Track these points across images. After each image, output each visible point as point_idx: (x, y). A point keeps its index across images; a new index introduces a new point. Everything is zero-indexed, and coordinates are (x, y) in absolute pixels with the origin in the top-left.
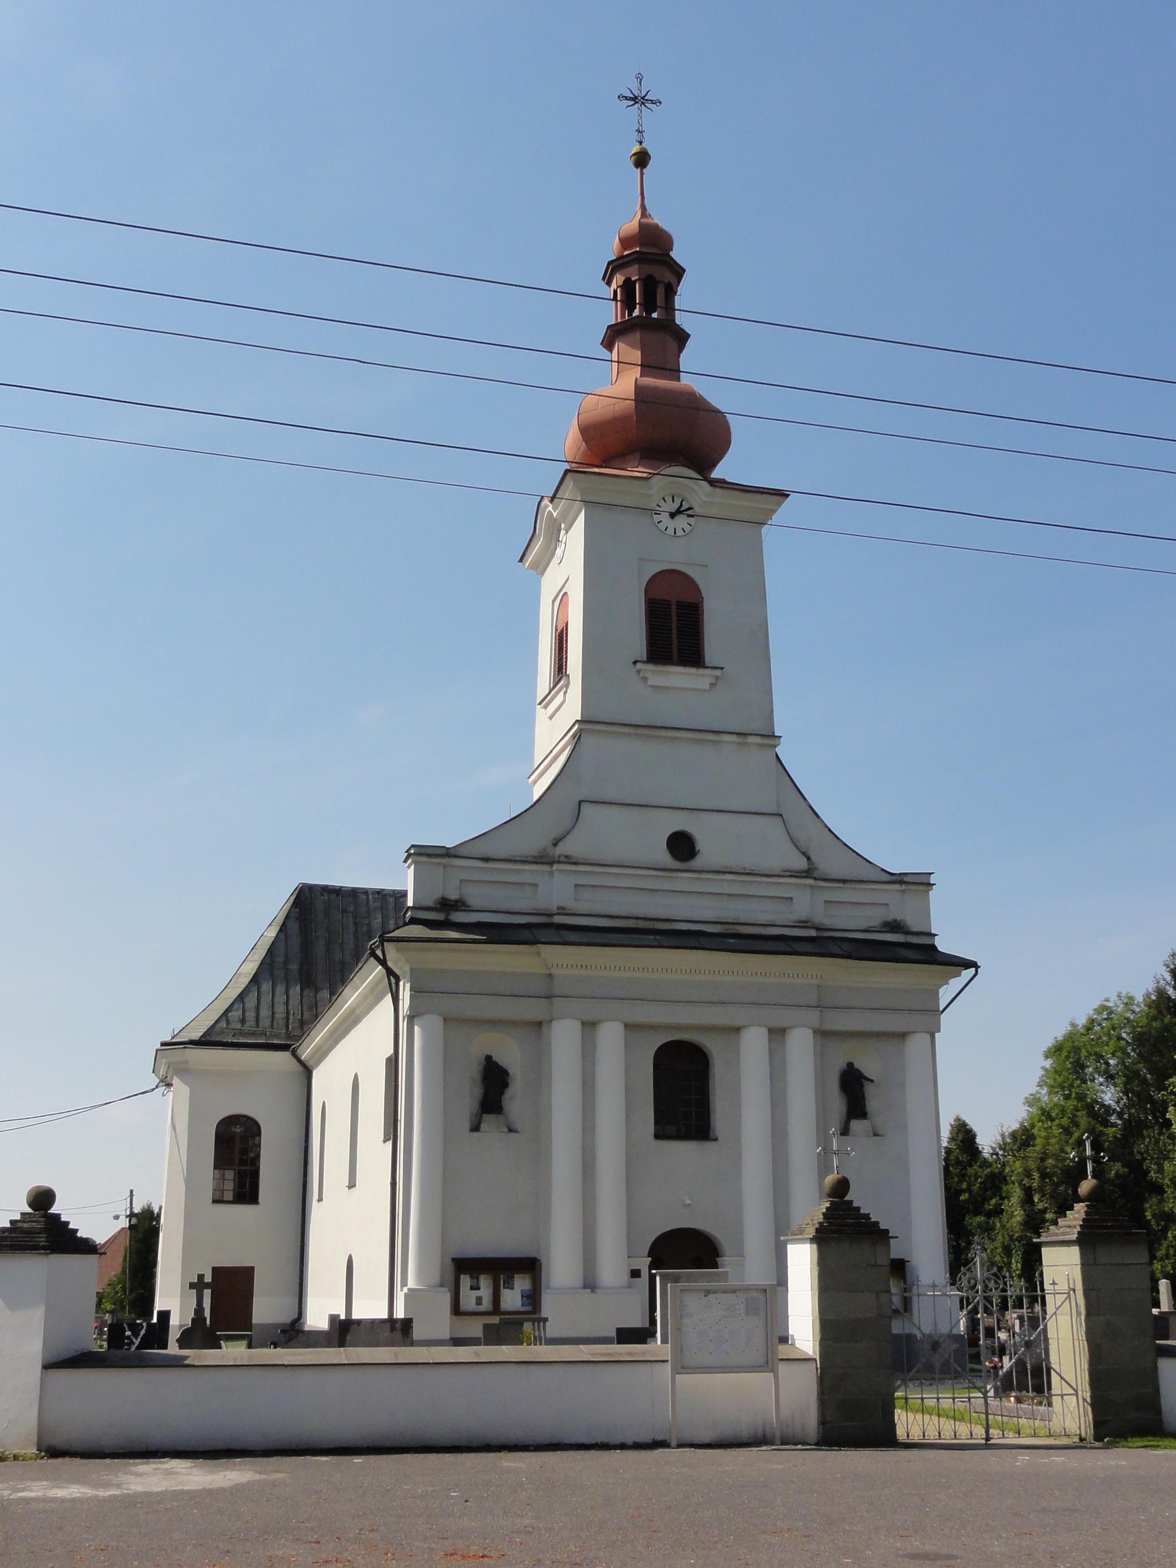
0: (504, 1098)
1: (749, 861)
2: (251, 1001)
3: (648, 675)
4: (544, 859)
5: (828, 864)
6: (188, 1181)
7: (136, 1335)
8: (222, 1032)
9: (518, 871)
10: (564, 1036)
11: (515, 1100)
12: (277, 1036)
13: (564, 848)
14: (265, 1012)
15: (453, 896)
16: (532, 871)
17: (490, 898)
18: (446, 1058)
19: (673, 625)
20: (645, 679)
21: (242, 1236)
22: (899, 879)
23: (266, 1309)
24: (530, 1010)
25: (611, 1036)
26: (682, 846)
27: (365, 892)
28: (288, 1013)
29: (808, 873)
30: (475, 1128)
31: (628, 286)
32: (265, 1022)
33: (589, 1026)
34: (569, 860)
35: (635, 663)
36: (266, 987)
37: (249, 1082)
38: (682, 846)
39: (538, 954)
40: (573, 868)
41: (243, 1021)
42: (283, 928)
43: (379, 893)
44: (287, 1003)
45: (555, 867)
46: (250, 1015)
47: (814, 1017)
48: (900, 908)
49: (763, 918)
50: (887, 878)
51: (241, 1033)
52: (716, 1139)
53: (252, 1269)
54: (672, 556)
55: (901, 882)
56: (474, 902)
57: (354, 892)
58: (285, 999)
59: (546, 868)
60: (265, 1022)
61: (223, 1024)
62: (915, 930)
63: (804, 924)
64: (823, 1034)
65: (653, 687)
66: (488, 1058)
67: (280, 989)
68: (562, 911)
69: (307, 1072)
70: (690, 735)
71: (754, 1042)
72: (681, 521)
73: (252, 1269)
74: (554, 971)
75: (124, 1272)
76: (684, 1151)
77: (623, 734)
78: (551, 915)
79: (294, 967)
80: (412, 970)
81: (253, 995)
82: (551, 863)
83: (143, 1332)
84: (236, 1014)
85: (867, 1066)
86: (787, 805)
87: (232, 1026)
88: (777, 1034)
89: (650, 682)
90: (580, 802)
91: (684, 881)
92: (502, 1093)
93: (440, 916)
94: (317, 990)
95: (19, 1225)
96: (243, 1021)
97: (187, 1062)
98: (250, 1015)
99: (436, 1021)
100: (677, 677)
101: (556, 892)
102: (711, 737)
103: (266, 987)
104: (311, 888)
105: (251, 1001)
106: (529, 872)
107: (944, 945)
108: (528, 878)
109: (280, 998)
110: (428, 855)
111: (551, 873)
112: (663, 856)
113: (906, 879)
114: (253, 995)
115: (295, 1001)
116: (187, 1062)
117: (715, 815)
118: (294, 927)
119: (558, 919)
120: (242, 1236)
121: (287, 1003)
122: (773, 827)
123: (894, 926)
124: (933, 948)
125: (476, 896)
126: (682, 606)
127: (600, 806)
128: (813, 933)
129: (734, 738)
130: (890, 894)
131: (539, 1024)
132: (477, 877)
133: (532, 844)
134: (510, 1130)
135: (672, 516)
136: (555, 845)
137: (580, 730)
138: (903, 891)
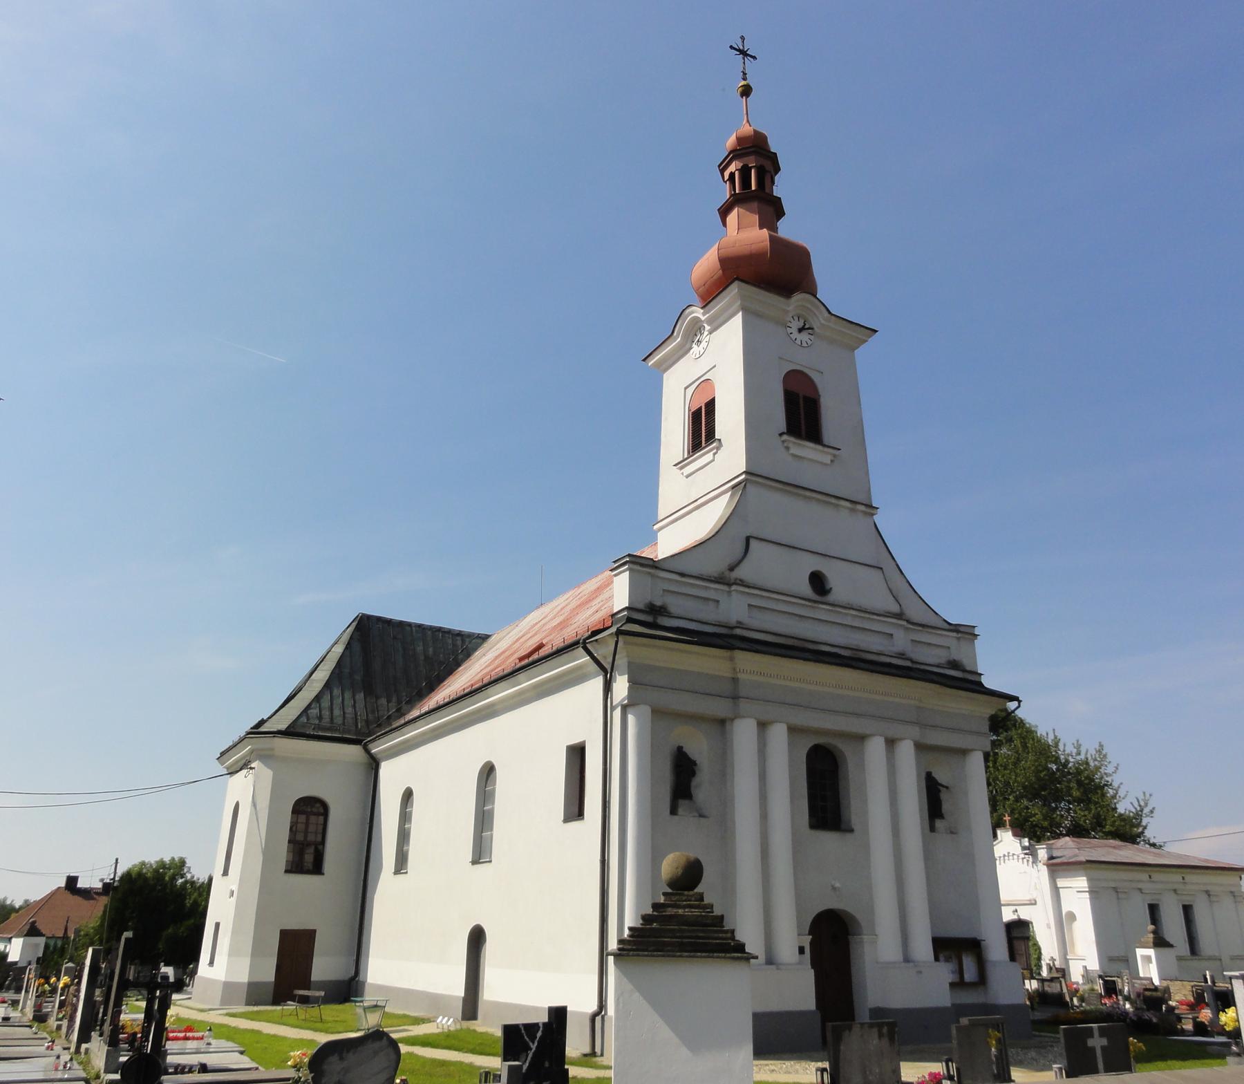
0: (694, 783)
1: (865, 602)
2: (326, 702)
3: (790, 445)
4: (720, 580)
5: (915, 613)
6: (265, 854)
7: (533, 1039)
8: (304, 726)
9: (706, 588)
10: (744, 732)
11: (703, 788)
12: (349, 732)
13: (739, 573)
14: (337, 712)
15: (658, 603)
16: (716, 589)
17: (686, 608)
18: (652, 743)
19: (799, 410)
20: (787, 448)
21: (312, 901)
22: (956, 628)
23: (324, 967)
24: (718, 708)
25: (778, 734)
26: (818, 582)
27: (409, 624)
28: (356, 714)
29: (900, 616)
30: (674, 811)
31: (745, 172)
32: (339, 721)
33: (762, 726)
34: (741, 583)
35: (781, 435)
36: (337, 692)
37: (326, 767)
38: (818, 582)
39: (732, 659)
40: (747, 590)
41: (320, 718)
42: (349, 646)
43: (420, 626)
44: (354, 706)
45: (734, 587)
46: (326, 713)
47: (915, 732)
48: (958, 652)
49: (875, 648)
50: (947, 627)
51: (319, 728)
52: (852, 831)
53: (315, 931)
54: (803, 360)
55: (958, 632)
56: (673, 610)
57: (401, 624)
58: (352, 705)
59: (725, 588)
60: (339, 721)
61: (304, 719)
62: (968, 668)
63: (901, 655)
64: (920, 747)
65: (794, 456)
66: (680, 749)
67: (348, 695)
68: (740, 625)
69: (374, 765)
70: (819, 497)
71: (875, 748)
72: (804, 337)
73: (315, 931)
74: (739, 676)
75: (102, 925)
76: (828, 839)
77: (771, 487)
78: (732, 628)
79: (358, 677)
80: (629, 663)
81: (327, 697)
82: (729, 585)
83: (539, 1034)
84: (314, 712)
85: (941, 776)
86: (883, 562)
87: (312, 721)
88: (891, 743)
89: (792, 451)
90: (748, 539)
91: (822, 612)
92: (689, 782)
93: (649, 619)
94: (377, 698)
95: (670, 911)
96: (320, 718)
97: (272, 749)
98: (326, 713)
99: (646, 710)
100: (807, 450)
101: (733, 609)
102: (833, 501)
103: (337, 692)
104: (369, 617)
105: (326, 702)
106: (714, 591)
107: (989, 682)
108: (711, 595)
109: (349, 702)
110: (642, 565)
111: (729, 592)
112: (807, 590)
113: (962, 629)
114: (327, 697)
115: (360, 704)
116: (272, 749)
117: (839, 562)
118: (357, 647)
119: (738, 632)
120: (312, 901)
121: (354, 706)
122: (876, 574)
123: (954, 665)
124: (981, 684)
125: (676, 605)
126: (806, 399)
127: (764, 544)
128: (908, 664)
129: (848, 504)
130: (950, 640)
131: (722, 722)
132: (672, 588)
133: (713, 566)
134: (701, 816)
135: (800, 330)
136: (732, 569)
137: (745, 480)
138: (958, 639)
